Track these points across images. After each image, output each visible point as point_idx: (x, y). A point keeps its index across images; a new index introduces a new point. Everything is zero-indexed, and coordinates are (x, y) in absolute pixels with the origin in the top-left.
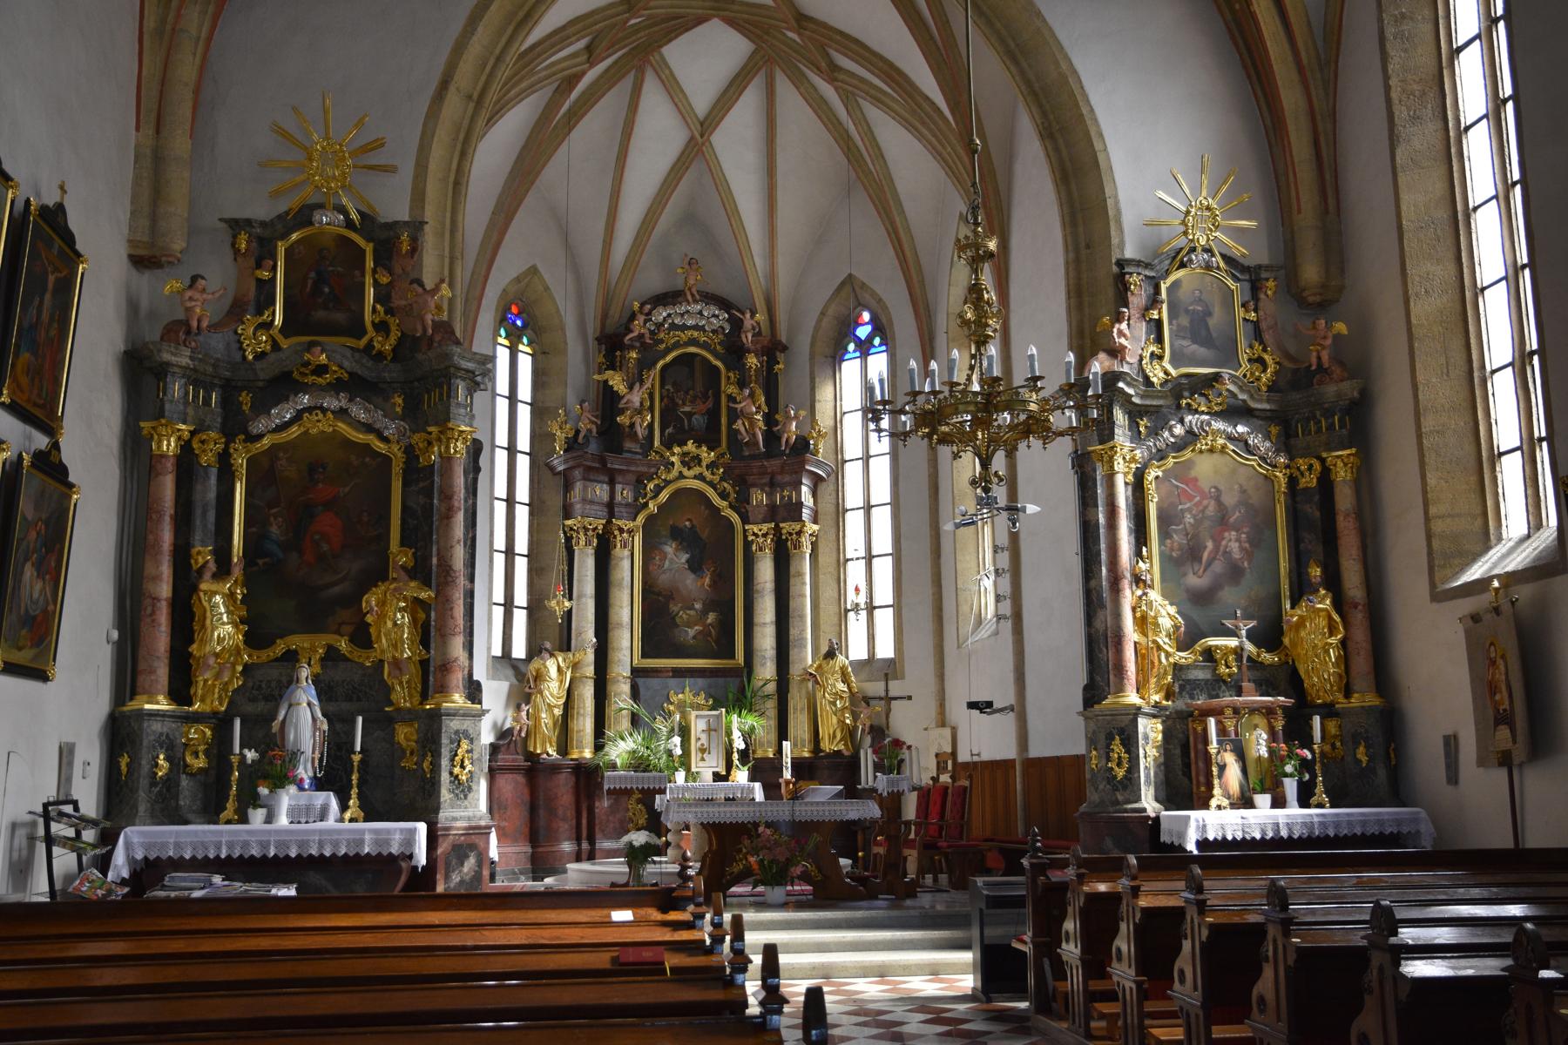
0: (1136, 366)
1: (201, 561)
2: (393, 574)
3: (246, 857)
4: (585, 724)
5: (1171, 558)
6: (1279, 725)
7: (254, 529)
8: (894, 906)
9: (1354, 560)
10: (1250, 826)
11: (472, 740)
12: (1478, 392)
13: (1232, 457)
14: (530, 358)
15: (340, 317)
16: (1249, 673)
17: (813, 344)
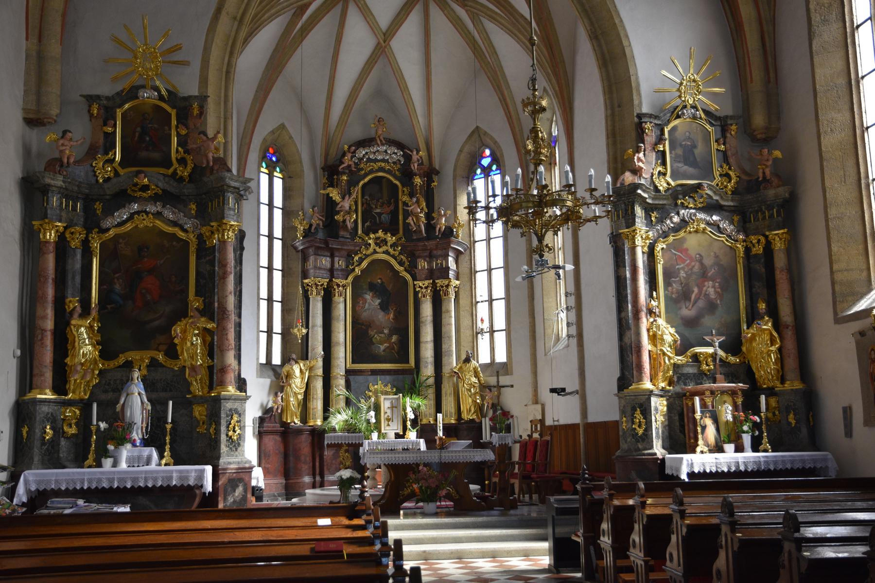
0: (649, 179)
1: (72, 306)
2: (191, 313)
3: (100, 488)
4: (317, 404)
5: (671, 298)
6: (740, 401)
7: (105, 287)
8: (503, 514)
9: (786, 298)
10: (721, 464)
11: (240, 415)
12: (864, 193)
13: (709, 235)
14: (281, 180)
15: (156, 155)
16: (721, 369)
17: (455, 170)
